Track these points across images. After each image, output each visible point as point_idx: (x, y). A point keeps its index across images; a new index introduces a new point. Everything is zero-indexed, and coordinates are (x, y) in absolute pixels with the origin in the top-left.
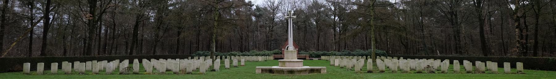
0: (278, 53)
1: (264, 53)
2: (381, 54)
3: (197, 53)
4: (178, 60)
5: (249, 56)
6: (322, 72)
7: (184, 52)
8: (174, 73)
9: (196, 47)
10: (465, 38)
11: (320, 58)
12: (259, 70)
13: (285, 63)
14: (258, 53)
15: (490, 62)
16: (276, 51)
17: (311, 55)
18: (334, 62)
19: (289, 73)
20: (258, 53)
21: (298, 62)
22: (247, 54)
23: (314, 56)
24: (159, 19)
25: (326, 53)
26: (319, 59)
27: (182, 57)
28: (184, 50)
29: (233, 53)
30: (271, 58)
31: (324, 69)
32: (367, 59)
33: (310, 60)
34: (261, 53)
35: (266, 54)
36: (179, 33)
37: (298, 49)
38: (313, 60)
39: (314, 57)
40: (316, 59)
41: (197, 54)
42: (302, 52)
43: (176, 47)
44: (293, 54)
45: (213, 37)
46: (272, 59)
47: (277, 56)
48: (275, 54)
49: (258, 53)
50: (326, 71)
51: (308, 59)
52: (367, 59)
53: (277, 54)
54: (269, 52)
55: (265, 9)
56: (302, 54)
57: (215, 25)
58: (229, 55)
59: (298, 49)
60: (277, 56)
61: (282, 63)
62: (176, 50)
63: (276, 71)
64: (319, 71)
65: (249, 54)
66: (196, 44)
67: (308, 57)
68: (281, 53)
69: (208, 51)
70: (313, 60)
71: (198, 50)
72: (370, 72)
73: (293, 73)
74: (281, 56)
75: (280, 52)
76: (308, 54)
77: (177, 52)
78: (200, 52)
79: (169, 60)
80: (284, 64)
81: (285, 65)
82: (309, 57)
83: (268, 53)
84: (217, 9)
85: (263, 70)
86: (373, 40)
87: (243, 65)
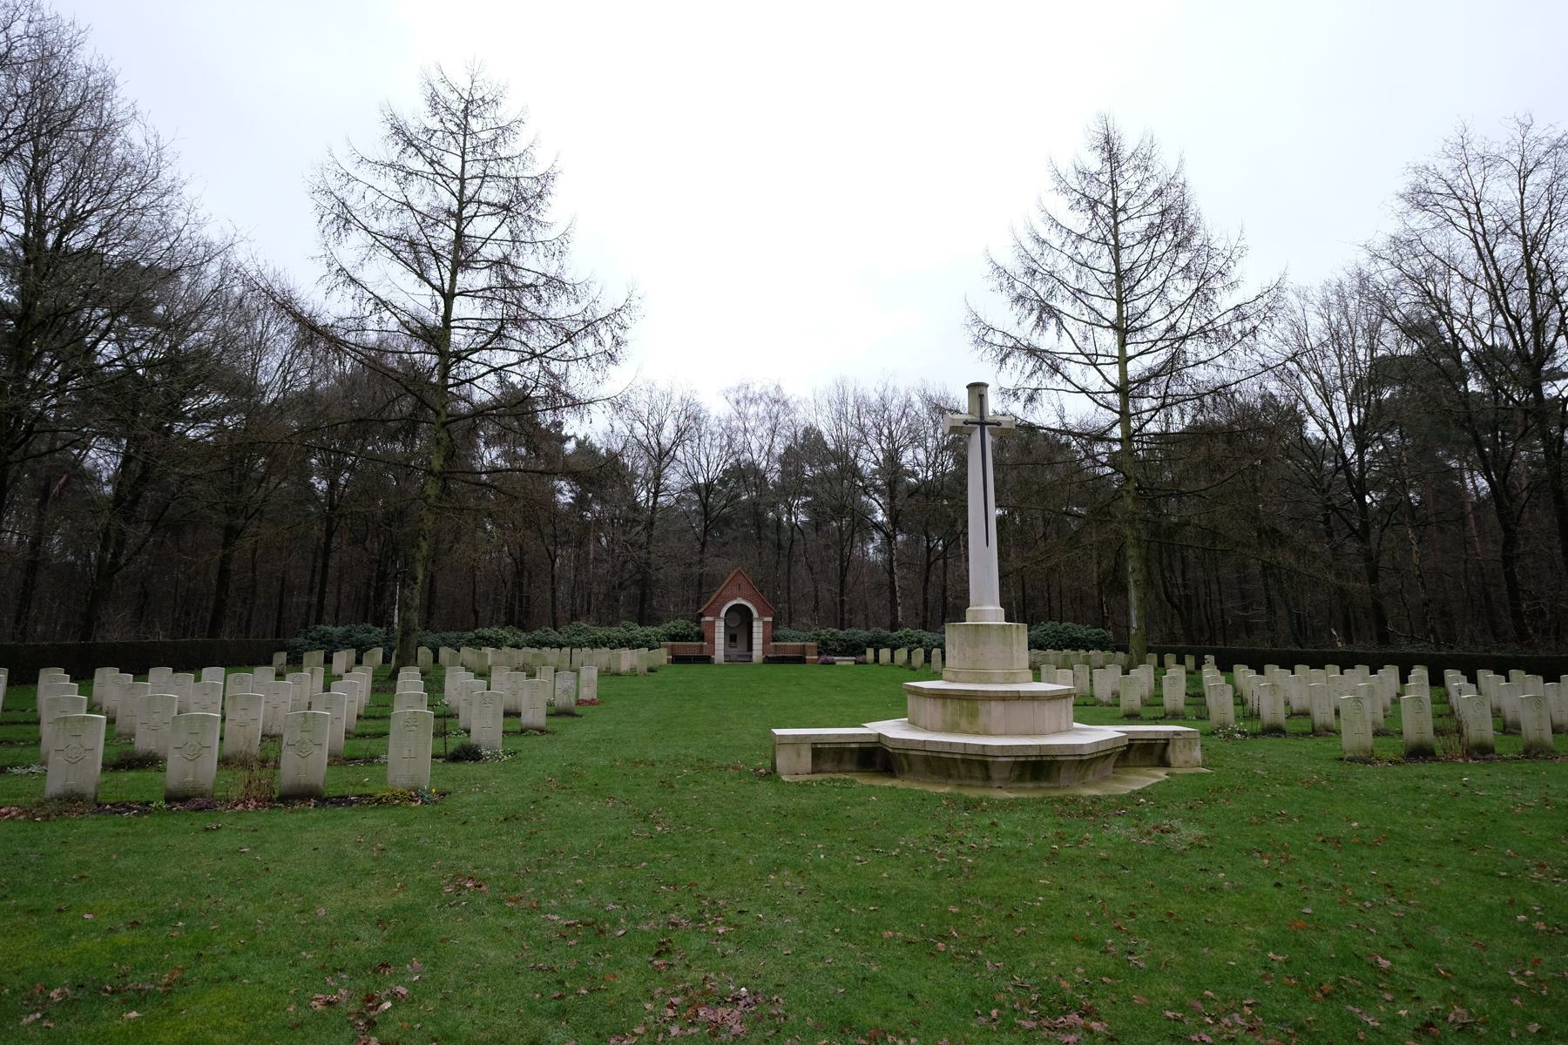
0: (688, 636)
1: (628, 635)
2: (1092, 642)
3: (313, 634)
4: (213, 675)
5: (560, 646)
6: (1177, 755)
7: (248, 628)
8: (168, 800)
9: (309, 606)
10: (1422, 583)
11: (861, 658)
12: (799, 755)
13: (983, 707)
14: (601, 632)
15: (1246, 668)
16: (679, 625)
17: (824, 643)
18: (1091, 680)
19: (1020, 778)
20: (601, 632)
21: (1053, 702)
22: (551, 638)
23: (839, 649)
24: (134, 477)
25: (884, 638)
26: (861, 663)
27: (242, 658)
28: (249, 620)
29: (486, 632)
30: (662, 655)
31: (1187, 739)
32: (1161, 664)
33: (823, 663)
34: (614, 632)
35: (635, 639)
36: (231, 534)
37: (770, 619)
38: (833, 663)
39: (835, 651)
40: (846, 662)
41: (314, 639)
42: (784, 631)
43: (211, 604)
44: (1015, 648)
45: (418, 556)
46: (665, 662)
47: (689, 648)
48: (673, 638)
49: (600, 634)
50: (1197, 754)
51: (814, 662)
52: (1161, 664)
53: (684, 638)
54: (649, 630)
55: (613, 457)
56: (786, 639)
57: (429, 496)
58: (470, 641)
59: (770, 619)
60: (689, 648)
61: (951, 706)
62: (209, 618)
63: (963, 761)
64: (1157, 751)
65: (561, 639)
66: (311, 590)
67: (815, 651)
68: (701, 637)
69: (369, 626)
70: (833, 663)
71: (319, 621)
72: (1420, 753)
73: (1048, 778)
74: (702, 646)
75: (697, 629)
76: (813, 640)
77: (215, 627)
78: (330, 628)
79: (160, 676)
80: (973, 715)
81: (982, 720)
82: (819, 654)
83: (647, 636)
84: (443, 419)
85: (824, 754)
86: (1135, 582)
87: (592, 702)
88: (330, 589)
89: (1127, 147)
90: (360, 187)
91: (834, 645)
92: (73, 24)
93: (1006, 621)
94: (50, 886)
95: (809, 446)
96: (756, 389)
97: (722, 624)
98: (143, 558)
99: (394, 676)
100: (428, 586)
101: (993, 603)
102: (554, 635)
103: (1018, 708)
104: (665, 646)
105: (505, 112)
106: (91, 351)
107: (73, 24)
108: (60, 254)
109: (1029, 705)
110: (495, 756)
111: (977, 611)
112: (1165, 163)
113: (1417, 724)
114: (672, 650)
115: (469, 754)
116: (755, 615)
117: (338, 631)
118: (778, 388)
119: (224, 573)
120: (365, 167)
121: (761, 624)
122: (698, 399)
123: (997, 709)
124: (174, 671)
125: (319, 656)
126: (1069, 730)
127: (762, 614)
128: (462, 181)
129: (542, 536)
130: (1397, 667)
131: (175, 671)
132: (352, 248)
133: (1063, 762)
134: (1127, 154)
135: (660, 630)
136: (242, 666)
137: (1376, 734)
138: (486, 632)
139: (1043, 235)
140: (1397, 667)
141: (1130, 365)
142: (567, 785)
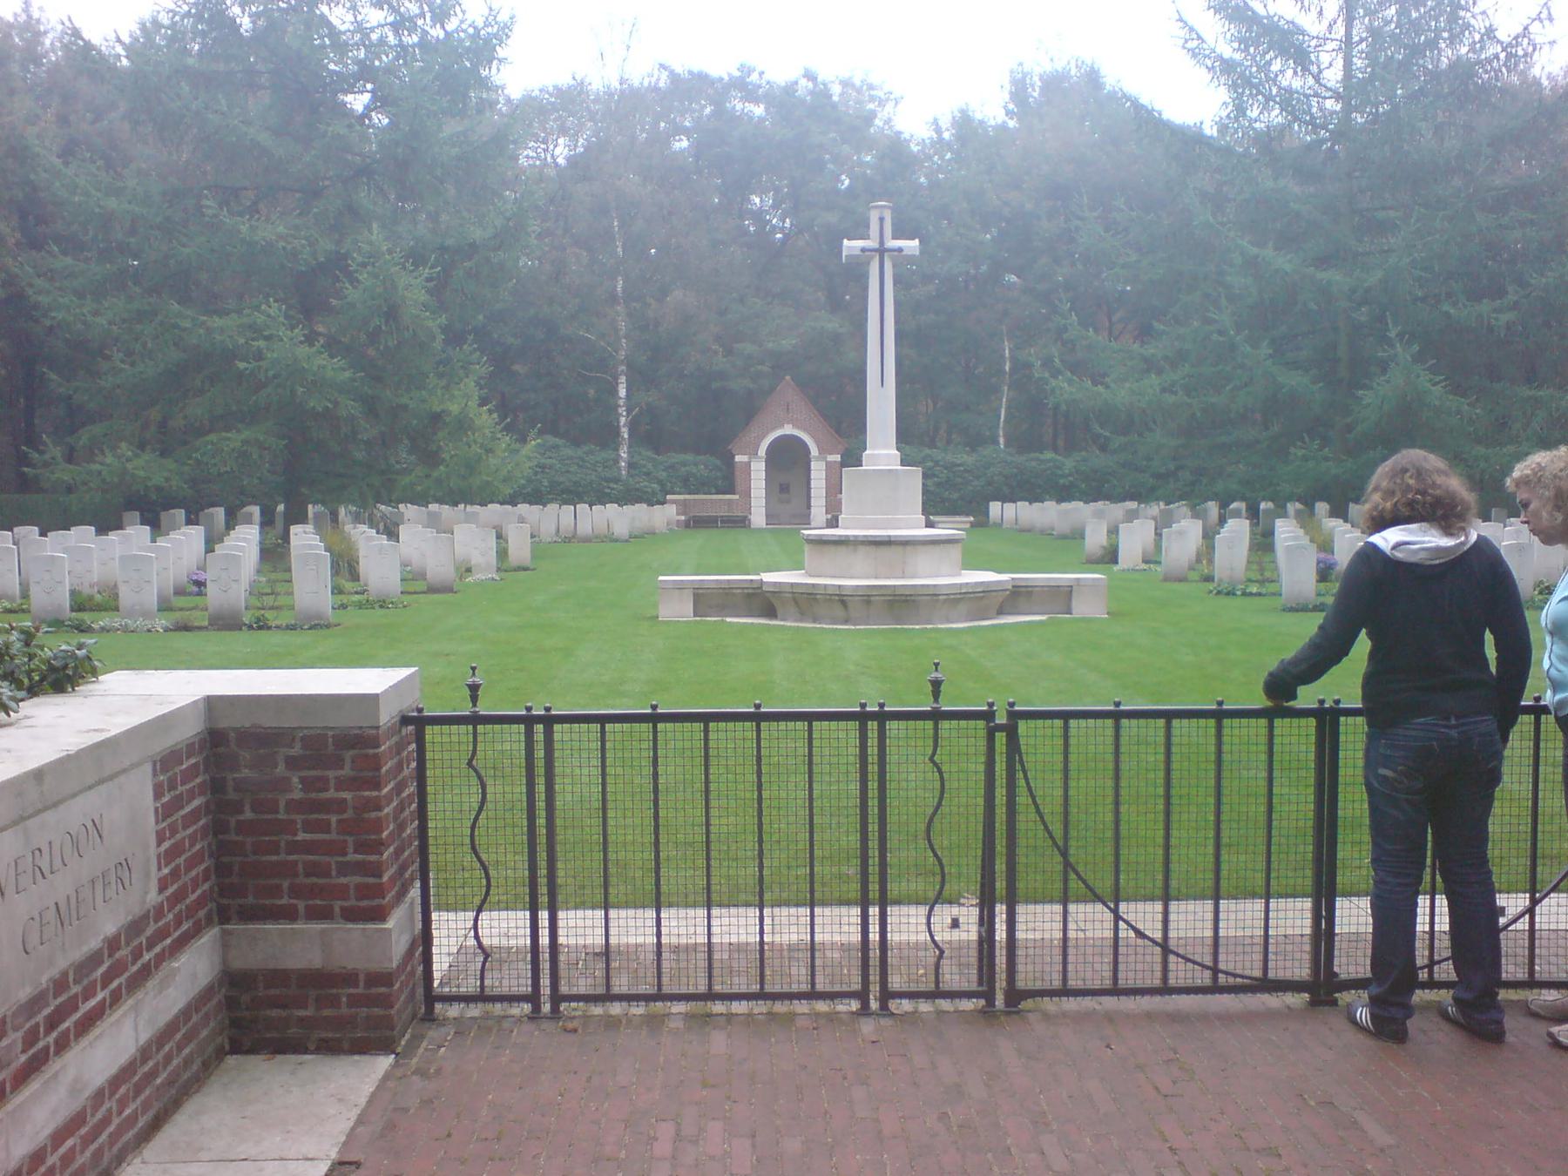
47: (714, 503)
85: (707, 601)
92: (590, 84)
93: (902, 465)
94: (830, 166)
97: (763, 465)
98: (377, 121)
99: (1269, 533)
101: (886, 447)
104: (674, 502)
107: (590, 84)
109: (900, 549)
111: (872, 455)
114: (684, 507)
116: (814, 451)
121: (823, 465)
124: (1030, 503)
126: (960, 575)
127: (823, 451)
130: (991, 503)
131: (1030, 503)
133: (702, 594)
136: (87, 958)
137: (1145, 561)
140: (991, 503)
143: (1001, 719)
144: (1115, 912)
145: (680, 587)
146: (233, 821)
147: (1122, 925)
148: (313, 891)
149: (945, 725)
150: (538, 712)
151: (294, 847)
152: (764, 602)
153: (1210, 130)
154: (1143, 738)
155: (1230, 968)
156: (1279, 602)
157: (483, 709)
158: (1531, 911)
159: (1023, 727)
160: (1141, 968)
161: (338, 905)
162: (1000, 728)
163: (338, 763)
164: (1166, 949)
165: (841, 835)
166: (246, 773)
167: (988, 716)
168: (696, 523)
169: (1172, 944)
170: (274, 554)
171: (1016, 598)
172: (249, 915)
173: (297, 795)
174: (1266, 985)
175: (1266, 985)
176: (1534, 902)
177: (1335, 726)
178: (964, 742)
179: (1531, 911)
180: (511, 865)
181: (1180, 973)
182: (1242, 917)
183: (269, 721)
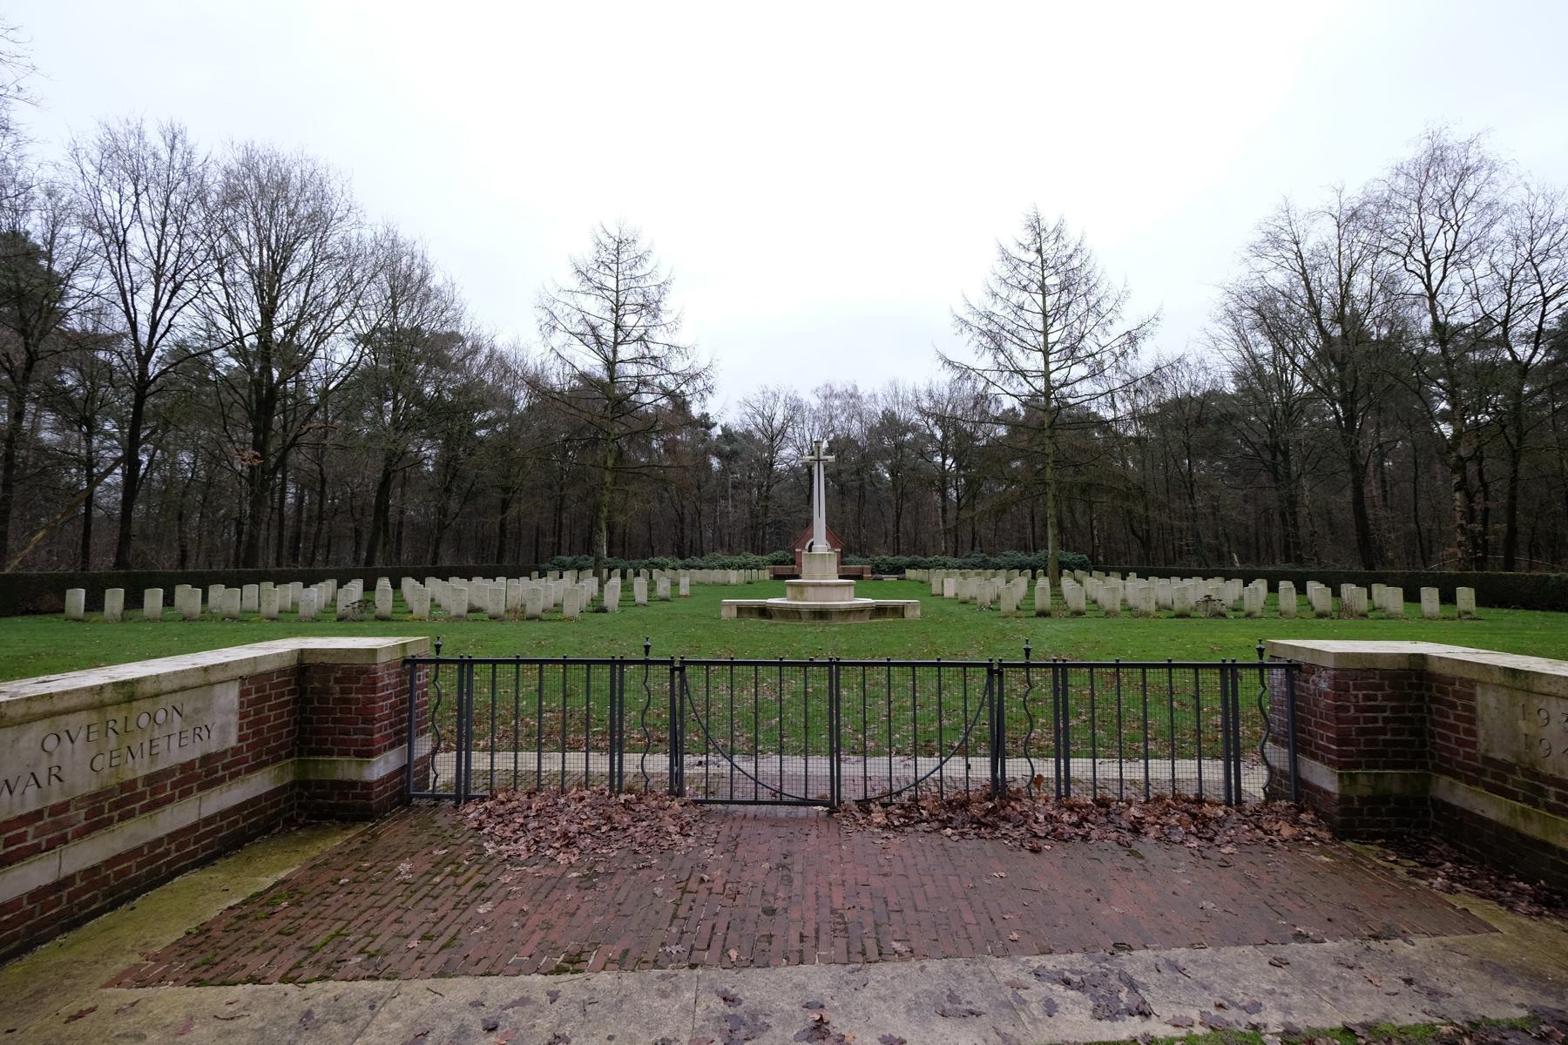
4: (501, 580)
6: (909, 614)
14: (727, 560)
16: (779, 554)
17: (877, 566)
24: (448, 465)
29: (656, 560)
30: (766, 574)
31: (914, 606)
34: (737, 560)
36: (505, 505)
40: (892, 578)
42: (851, 558)
43: (497, 544)
48: (775, 563)
50: (919, 612)
53: (782, 563)
54: (758, 558)
56: (851, 563)
61: (795, 589)
65: (702, 564)
68: (793, 562)
72: (1043, 614)
77: (500, 559)
80: (802, 593)
82: (873, 573)
85: (741, 610)
88: (565, 531)
89: (1049, 223)
90: (560, 305)
91: (884, 567)
95: (890, 424)
96: (838, 388)
100: (38, 708)
102: (698, 561)
103: (824, 590)
105: (641, 247)
106: (420, 392)
108: (750, 1022)
110: (614, 611)
112: (1072, 236)
113: (1043, 599)
115: (603, 610)
117: (568, 559)
118: (855, 387)
119: (502, 525)
120: (562, 294)
122: (799, 396)
123: (811, 590)
125: (557, 573)
128: (617, 292)
129: (1304, 271)
132: (559, 339)
134: (1049, 229)
135: (766, 558)
138: (656, 560)
139: (996, 290)
141: (1053, 376)
142: (1376, 981)
143: (677, 665)
144: (731, 761)
145: (730, 604)
146: (308, 707)
147: (736, 772)
148: (344, 742)
149: (785, 669)
150: (617, 658)
151: (335, 721)
152: (764, 612)
153: (1231, 388)
154: (506, 673)
155: (790, 793)
156: (1173, 614)
157: (650, 658)
158: (940, 767)
159: (688, 670)
160: (745, 790)
161: (352, 749)
162: (677, 669)
163: (358, 681)
164: (757, 782)
165: (984, 726)
166: (316, 685)
167: (671, 662)
168: (778, 577)
169: (760, 779)
170: (627, 588)
171: (880, 611)
172: (313, 752)
173: (338, 696)
174: (805, 802)
175: (805, 802)
176: (942, 763)
177: (1235, 677)
178: (1042, 681)
179: (940, 767)
180: (1042, 733)
181: (764, 795)
182: (794, 765)
183: (326, 660)
